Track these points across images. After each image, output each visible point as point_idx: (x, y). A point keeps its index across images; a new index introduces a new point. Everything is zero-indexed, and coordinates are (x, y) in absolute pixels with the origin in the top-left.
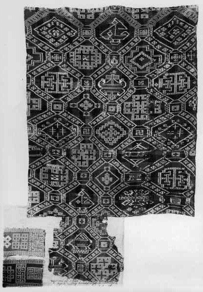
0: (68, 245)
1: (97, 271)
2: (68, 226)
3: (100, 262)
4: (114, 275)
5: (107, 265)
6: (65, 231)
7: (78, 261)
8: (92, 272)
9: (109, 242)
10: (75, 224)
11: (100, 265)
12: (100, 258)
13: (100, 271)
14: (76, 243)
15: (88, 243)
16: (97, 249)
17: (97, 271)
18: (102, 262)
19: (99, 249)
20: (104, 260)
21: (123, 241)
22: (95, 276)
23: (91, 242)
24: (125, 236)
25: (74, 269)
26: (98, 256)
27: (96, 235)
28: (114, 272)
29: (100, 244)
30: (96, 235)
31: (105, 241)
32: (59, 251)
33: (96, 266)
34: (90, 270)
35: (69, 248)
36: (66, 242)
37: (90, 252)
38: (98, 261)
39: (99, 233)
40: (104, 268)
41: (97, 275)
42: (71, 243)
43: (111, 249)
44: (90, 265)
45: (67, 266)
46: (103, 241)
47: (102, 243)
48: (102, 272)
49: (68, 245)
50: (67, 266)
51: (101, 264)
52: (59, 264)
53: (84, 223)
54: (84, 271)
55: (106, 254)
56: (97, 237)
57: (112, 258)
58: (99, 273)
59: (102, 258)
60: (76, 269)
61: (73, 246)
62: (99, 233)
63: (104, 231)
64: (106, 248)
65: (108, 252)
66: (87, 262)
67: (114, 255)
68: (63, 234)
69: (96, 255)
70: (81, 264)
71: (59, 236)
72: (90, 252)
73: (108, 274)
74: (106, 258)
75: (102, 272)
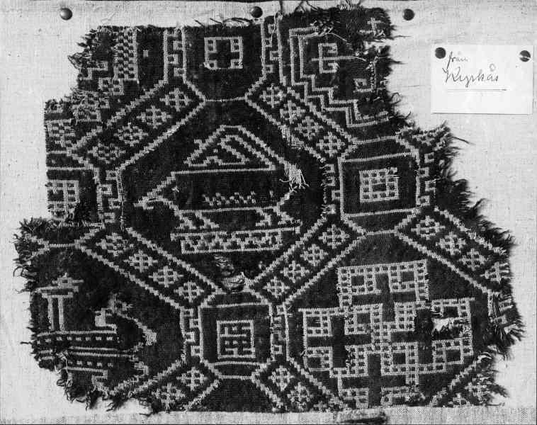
0: (143, 203)
1: (341, 358)
2: (132, 90)
3: (357, 300)
4: (457, 369)
5: (405, 316)
6: (120, 115)
7: (219, 299)
8: (315, 362)
9: (406, 170)
10: (182, 73)
11: (364, 318)
12: (358, 270)
13: (361, 355)
14: (194, 192)
15: (277, 182)
16: (335, 220)
17: (341, 358)
18: (370, 300)
19: (345, 217)
20: (382, 280)
21: (464, 141)
22: (332, 384)
23: (295, 174)
24: (400, 65)
25: (199, 351)
26: (347, 261)
27: (323, 133)
28: (454, 355)
29: (352, 186)
30: (323, 133)
31: (381, 164)
32: (209, 290)
33: (338, 323)
34: (297, 350)
35: (158, 225)
36: (135, 184)
37: (290, 238)
38: (346, 290)
39: (340, 118)
40: (385, 331)
41: (347, 383)
42: (167, 192)
43: (427, 211)
44: (296, 321)
45: (151, 337)
46: (370, 166)
47: (369, 179)
48: (375, 361)
49: (143, 203)
50: (151, 337)
51: (364, 309)
52: (100, 321)
53: (237, 64)
54: (264, 354)
55: (397, 243)
56: (331, 144)
57: (434, 266)
58: (360, 368)
59: (371, 272)
60: (211, 355)
61: (179, 213)
62: (340, 118)
63: (382, 100)
64: (393, 204)
65: (407, 231)
66: (277, 302)
67: (451, 244)
68: (108, 137)
69: (332, 253)
70: (241, 313)
71: (82, 152)
72: (290, 238)
73: (414, 371)
74: (393, 271)
75: (375, 361)
